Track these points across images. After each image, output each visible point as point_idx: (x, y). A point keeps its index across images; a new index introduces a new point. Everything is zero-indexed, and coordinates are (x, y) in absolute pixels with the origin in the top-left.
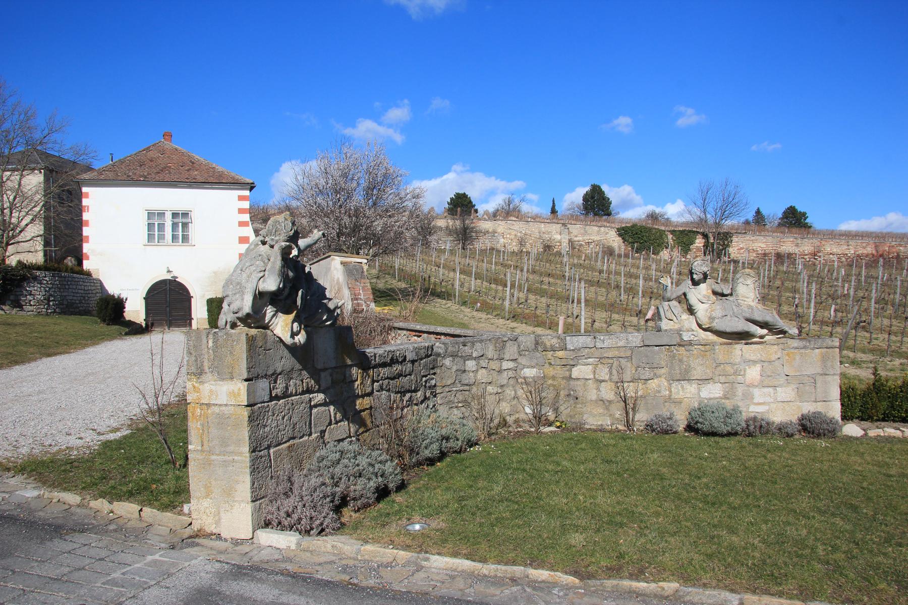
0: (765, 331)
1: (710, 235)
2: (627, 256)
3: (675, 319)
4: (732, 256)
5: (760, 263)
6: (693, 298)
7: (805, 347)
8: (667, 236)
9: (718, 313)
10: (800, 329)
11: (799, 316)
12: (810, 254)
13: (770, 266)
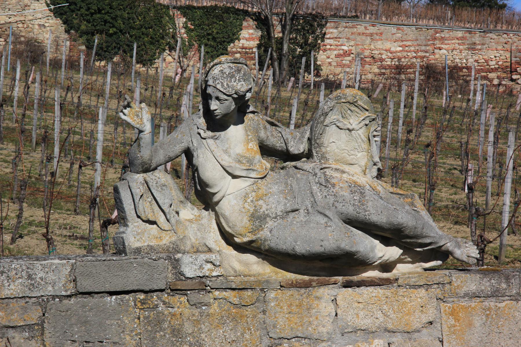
0: (394, 252)
1: (275, 21)
2: (72, 65)
3: (161, 219)
4: (325, 71)
5: (387, 89)
6: (210, 169)
7: (496, 294)
8: (172, 19)
9: (274, 203)
10: (482, 244)
11: (478, 214)
12: (503, 69)
13: (410, 95)
